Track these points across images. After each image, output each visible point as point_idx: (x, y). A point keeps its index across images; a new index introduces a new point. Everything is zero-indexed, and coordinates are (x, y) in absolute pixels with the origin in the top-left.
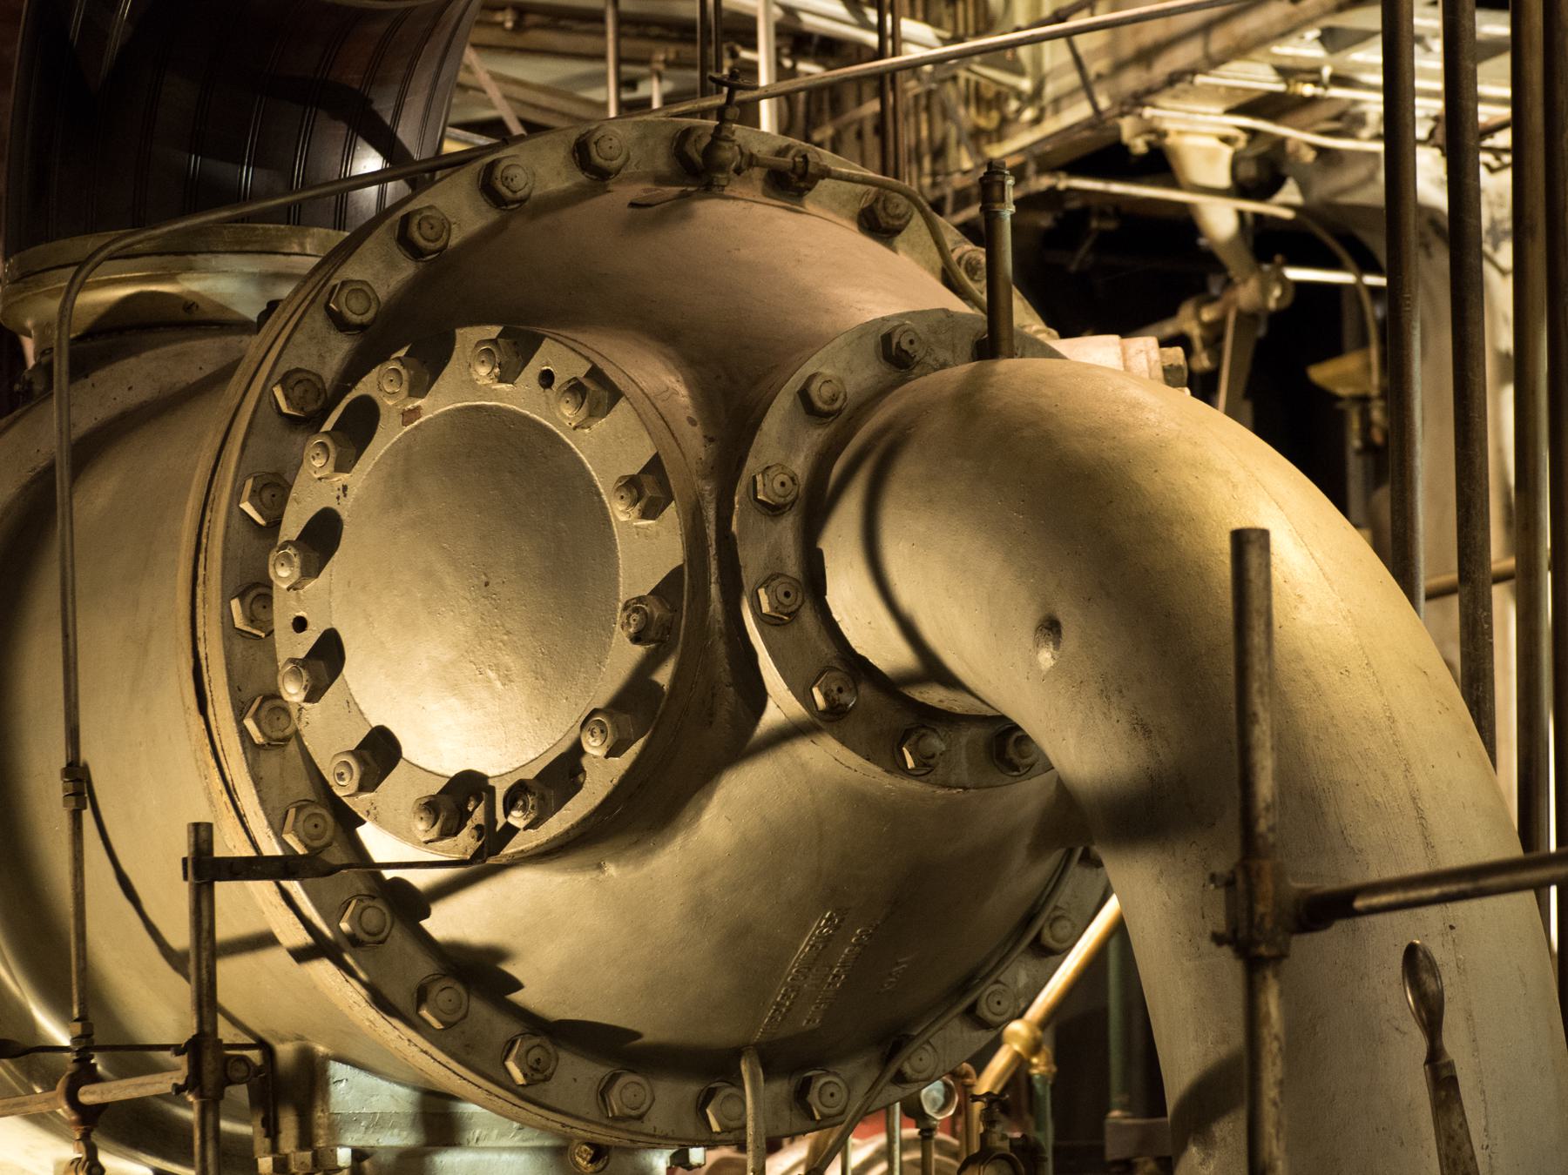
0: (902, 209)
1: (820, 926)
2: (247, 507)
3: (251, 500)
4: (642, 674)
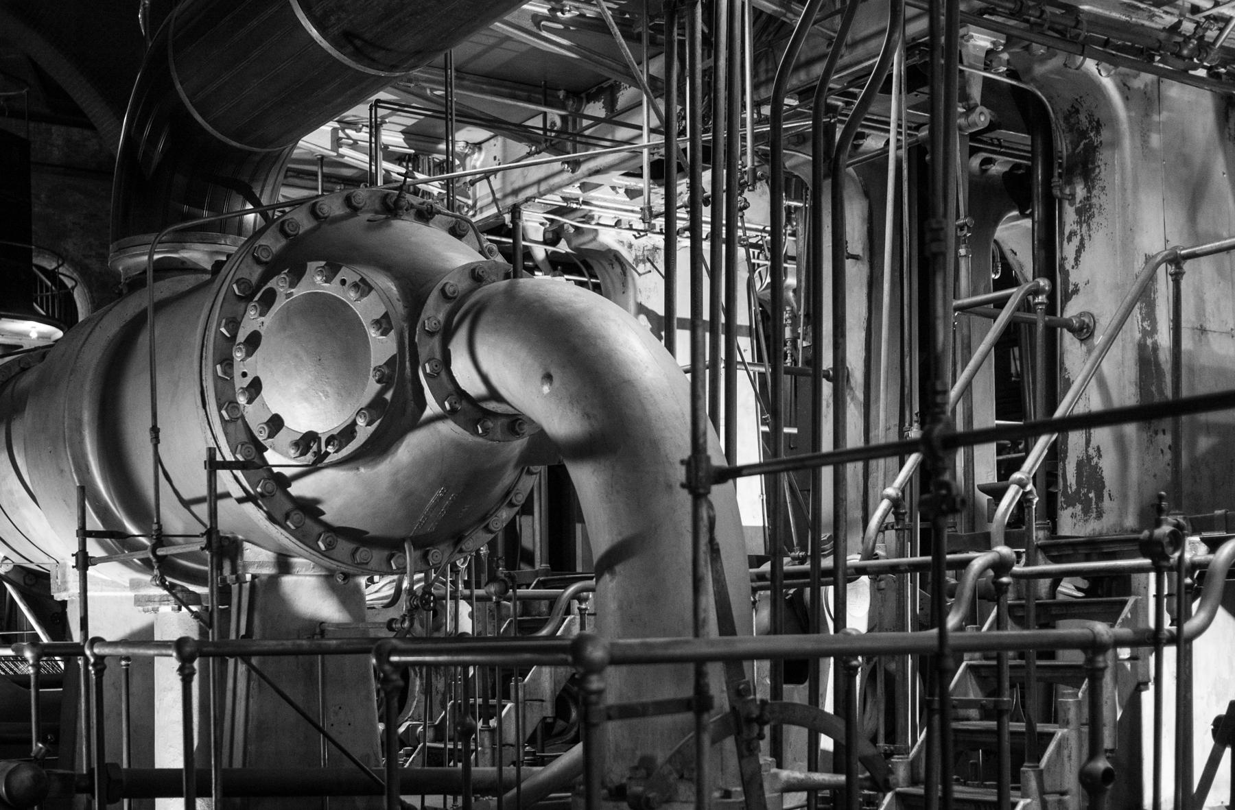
0: (465, 228)
1: (439, 493)
2: (223, 330)
3: (225, 327)
4: (379, 397)
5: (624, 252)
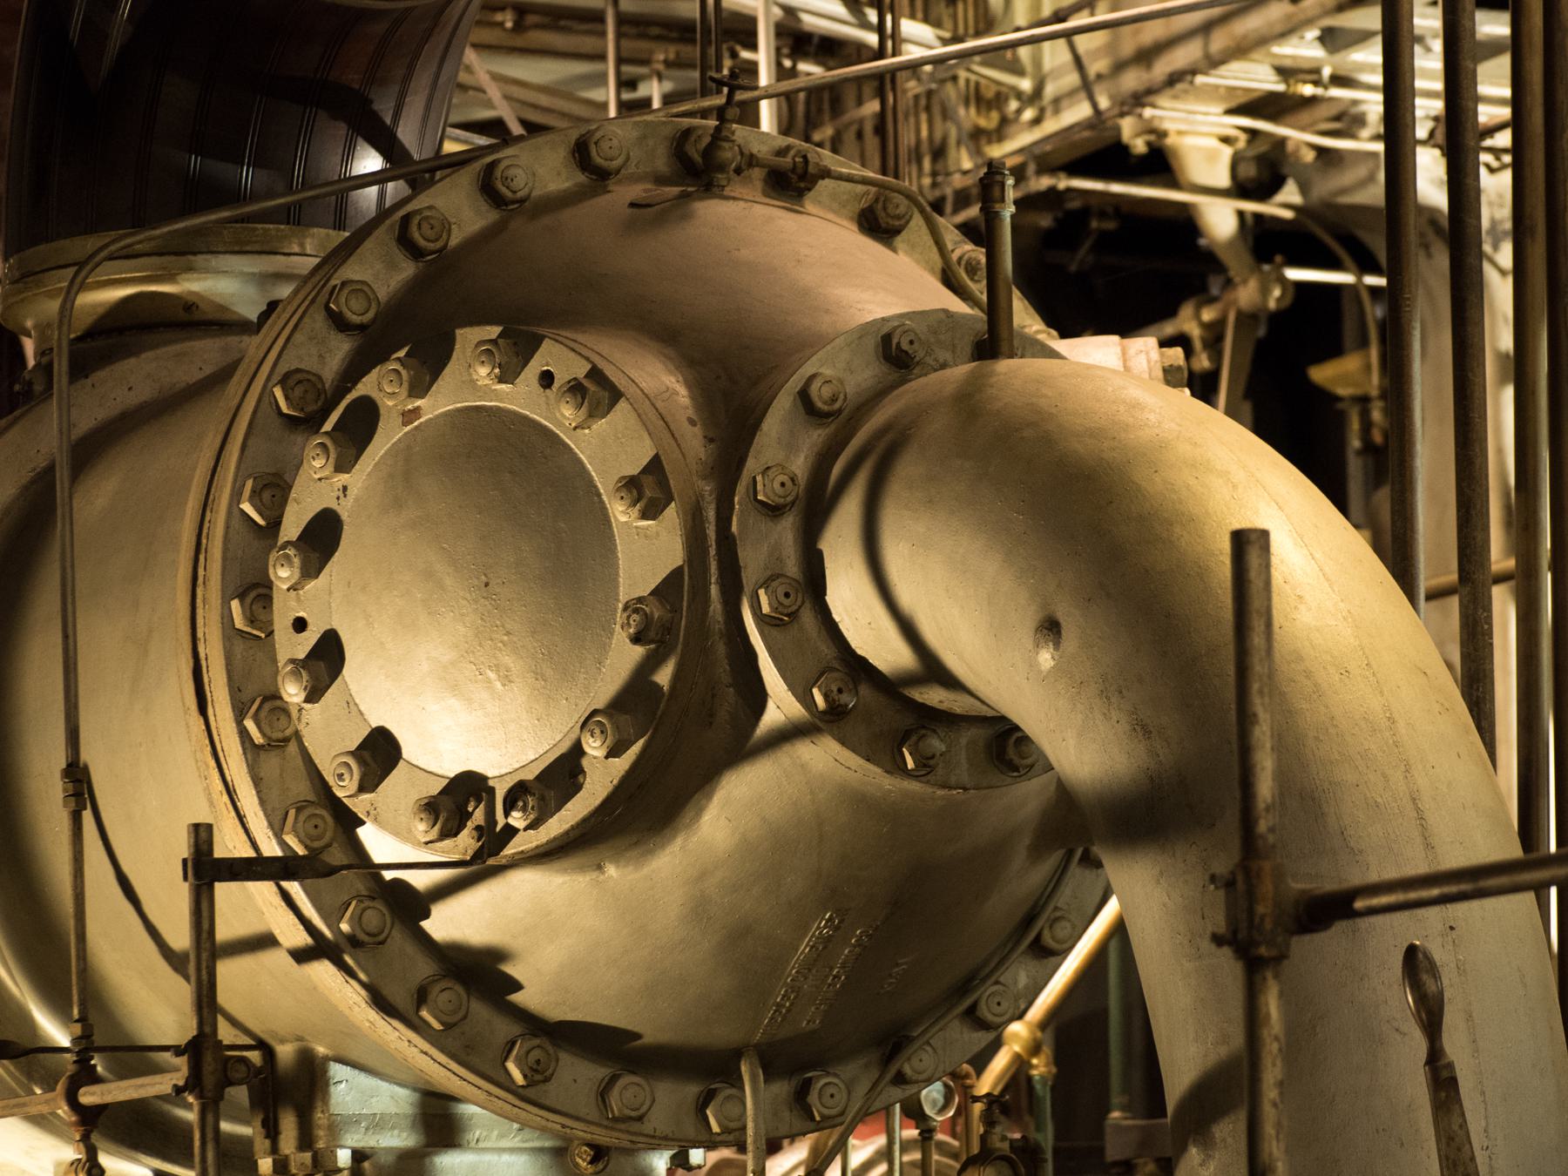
0: (902, 210)
1: (820, 926)
2: (247, 507)
3: (251, 500)
4: (642, 675)
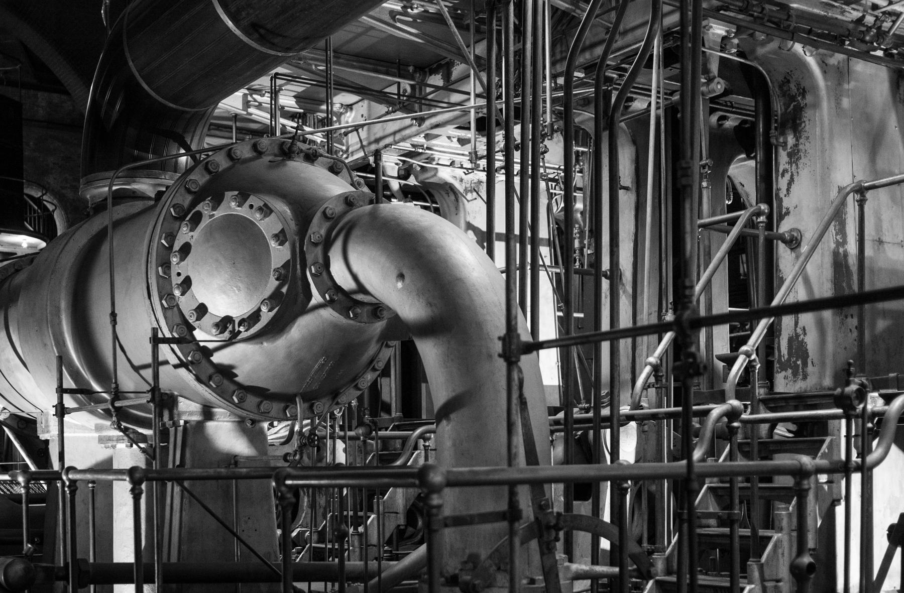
0: (341, 167)
1: (321, 361)
2: (163, 241)
3: (165, 240)
4: (277, 291)
5: (457, 185)
